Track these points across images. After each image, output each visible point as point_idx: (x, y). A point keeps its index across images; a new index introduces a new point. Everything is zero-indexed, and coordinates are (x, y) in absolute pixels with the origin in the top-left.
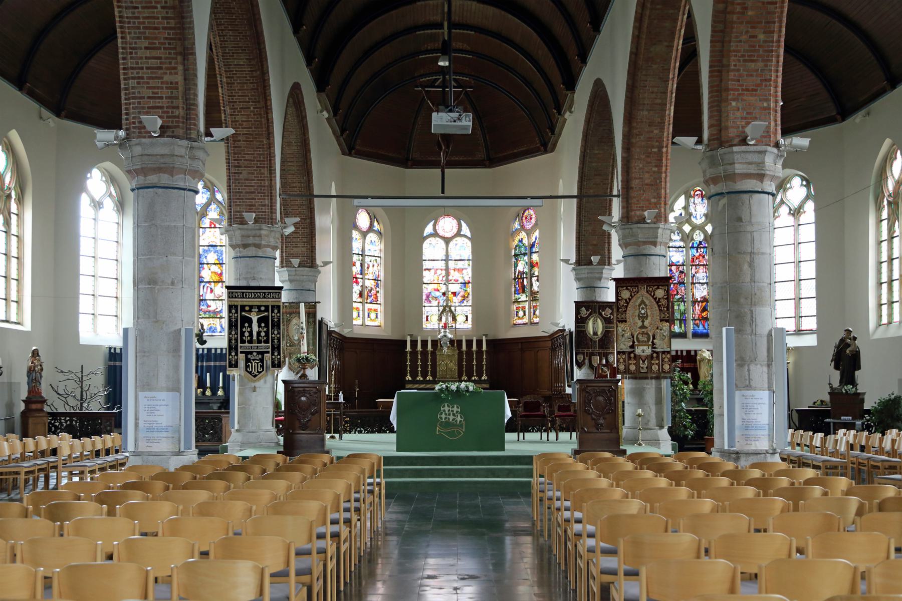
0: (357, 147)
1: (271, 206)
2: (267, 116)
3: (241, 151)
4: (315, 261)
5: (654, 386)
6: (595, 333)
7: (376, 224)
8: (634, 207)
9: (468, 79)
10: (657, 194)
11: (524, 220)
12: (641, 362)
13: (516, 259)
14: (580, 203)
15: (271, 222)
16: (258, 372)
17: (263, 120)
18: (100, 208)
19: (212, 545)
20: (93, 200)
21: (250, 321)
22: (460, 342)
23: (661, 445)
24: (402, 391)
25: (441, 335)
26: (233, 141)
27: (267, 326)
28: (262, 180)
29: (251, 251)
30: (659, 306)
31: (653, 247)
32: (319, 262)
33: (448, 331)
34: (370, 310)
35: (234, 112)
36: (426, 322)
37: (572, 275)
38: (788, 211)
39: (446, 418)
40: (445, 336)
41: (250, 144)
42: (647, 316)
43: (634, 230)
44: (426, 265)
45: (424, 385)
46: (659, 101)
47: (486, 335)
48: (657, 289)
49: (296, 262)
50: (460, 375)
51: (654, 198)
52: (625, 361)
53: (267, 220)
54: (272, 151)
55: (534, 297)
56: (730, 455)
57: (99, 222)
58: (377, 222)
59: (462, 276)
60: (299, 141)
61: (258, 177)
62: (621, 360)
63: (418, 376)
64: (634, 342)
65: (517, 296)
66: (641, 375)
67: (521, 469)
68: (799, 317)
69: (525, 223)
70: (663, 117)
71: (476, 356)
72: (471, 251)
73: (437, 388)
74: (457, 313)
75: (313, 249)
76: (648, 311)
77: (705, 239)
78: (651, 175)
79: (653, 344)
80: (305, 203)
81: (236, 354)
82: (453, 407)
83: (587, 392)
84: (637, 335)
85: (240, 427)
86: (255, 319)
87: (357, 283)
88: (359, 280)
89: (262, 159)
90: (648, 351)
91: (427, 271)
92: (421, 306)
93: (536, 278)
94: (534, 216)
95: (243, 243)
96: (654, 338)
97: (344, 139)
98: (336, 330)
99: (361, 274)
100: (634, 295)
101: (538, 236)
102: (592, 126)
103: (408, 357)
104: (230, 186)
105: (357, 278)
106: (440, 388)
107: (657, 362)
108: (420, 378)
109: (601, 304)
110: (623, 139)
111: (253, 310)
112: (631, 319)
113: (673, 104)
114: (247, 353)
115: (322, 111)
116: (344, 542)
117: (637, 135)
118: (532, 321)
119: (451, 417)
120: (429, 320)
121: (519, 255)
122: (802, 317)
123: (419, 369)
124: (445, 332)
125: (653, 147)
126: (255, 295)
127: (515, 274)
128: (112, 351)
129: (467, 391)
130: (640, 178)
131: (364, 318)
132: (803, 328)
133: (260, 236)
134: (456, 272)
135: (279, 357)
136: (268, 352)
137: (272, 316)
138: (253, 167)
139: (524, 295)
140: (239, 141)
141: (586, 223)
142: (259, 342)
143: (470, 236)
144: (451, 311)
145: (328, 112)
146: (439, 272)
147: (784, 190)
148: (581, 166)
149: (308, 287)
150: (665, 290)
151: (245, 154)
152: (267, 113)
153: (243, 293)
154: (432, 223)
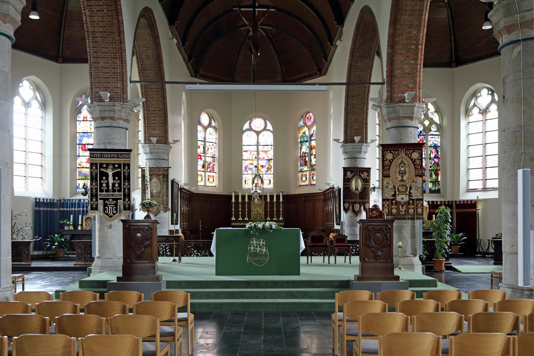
0: (201, 72)
1: (123, 88)
2: (118, 18)
3: (98, 45)
4: (168, 140)
5: (410, 225)
6: (357, 189)
7: (213, 122)
8: (396, 91)
9: (271, 28)
10: (414, 81)
11: (306, 120)
12: (401, 207)
13: (301, 145)
14: (347, 101)
15: (123, 101)
16: (113, 214)
17: (114, 20)
18: (29, 107)
19: (135, 306)
20: (24, 101)
21: (107, 175)
22: (266, 197)
23: (415, 269)
24: (220, 228)
25: (253, 191)
26: (92, 37)
27: (120, 179)
28: (115, 68)
29: (108, 122)
30: (415, 165)
31: (410, 121)
32: (170, 140)
33: (258, 188)
34: (209, 176)
35: (92, 14)
36: (244, 184)
37: (341, 150)
38: (479, 111)
39: (254, 250)
40: (256, 191)
41: (106, 40)
42: (406, 172)
43: (396, 108)
44: (245, 148)
45: (243, 223)
46: (418, 8)
47: (282, 192)
48: (413, 152)
49: (154, 140)
50: (266, 217)
51: (412, 84)
52: (388, 206)
53: (119, 99)
54: (123, 46)
55: (312, 168)
56: (522, 292)
57: (28, 116)
58: (214, 120)
59: (267, 155)
60: (155, 54)
61: (112, 66)
62: (386, 205)
63: (239, 218)
64: (395, 192)
65: (302, 168)
66: (401, 217)
67: (315, 292)
68: (485, 180)
69: (307, 121)
70: (420, 21)
71: (276, 205)
72: (273, 140)
73: (247, 227)
74: (264, 178)
75: (166, 131)
76: (406, 169)
77: (424, 130)
78: (409, 67)
79: (410, 193)
80: (160, 99)
81: (97, 200)
82: (260, 241)
83: (368, 230)
84: (398, 187)
85: (100, 254)
86: (110, 174)
87: (201, 159)
88: (202, 157)
89: (115, 52)
90: (406, 198)
91: (245, 152)
92: (242, 174)
93: (314, 156)
94: (312, 117)
95: (101, 116)
96: (410, 189)
97: (190, 64)
98: (186, 187)
99: (204, 153)
100: (396, 157)
101: (315, 130)
102: (357, 45)
103: (233, 206)
104: (91, 73)
105: (201, 156)
106: (250, 226)
107: (413, 207)
108: (240, 219)
109: (360, 169)
110: (389, 38)
111: (109, 167)
112: (393, 174)
113: (428, 11)
114: (105, 200)
115: (172, 39)
116: (191, 323)
117: (400, 35)
118: (311, 183)
119: (258, 249)
120: (246, 182)
121: (303, 142)
122: (487, 179)
123: (240, 213)
124: (256, 189)
125: (412, 45)
126: (111, 156)
127: (300, 154)
128: (38, 200)
129: (271, 228)
130: (401, 69)
131: (205, 181)
132: (488, 187)
133: (114, 111)
134: (264, 153)
135: (129, 202)
136: (121, 199)
137: (124, 172)
138: (109, 58)
139: (306, 167)
140: (97, 37)
141: (351, 115)
142: (114, 191)
143: (272, 130)
144: (260, 177)
145: (177, 39)
146: (253, 153)
147: (476, 98)
148: (349, 74)
149: (162, 157)
150: (419, 153)
151: (101, 47)
152: (118, 16)
153: (101, 154)
154: (249, 122)
